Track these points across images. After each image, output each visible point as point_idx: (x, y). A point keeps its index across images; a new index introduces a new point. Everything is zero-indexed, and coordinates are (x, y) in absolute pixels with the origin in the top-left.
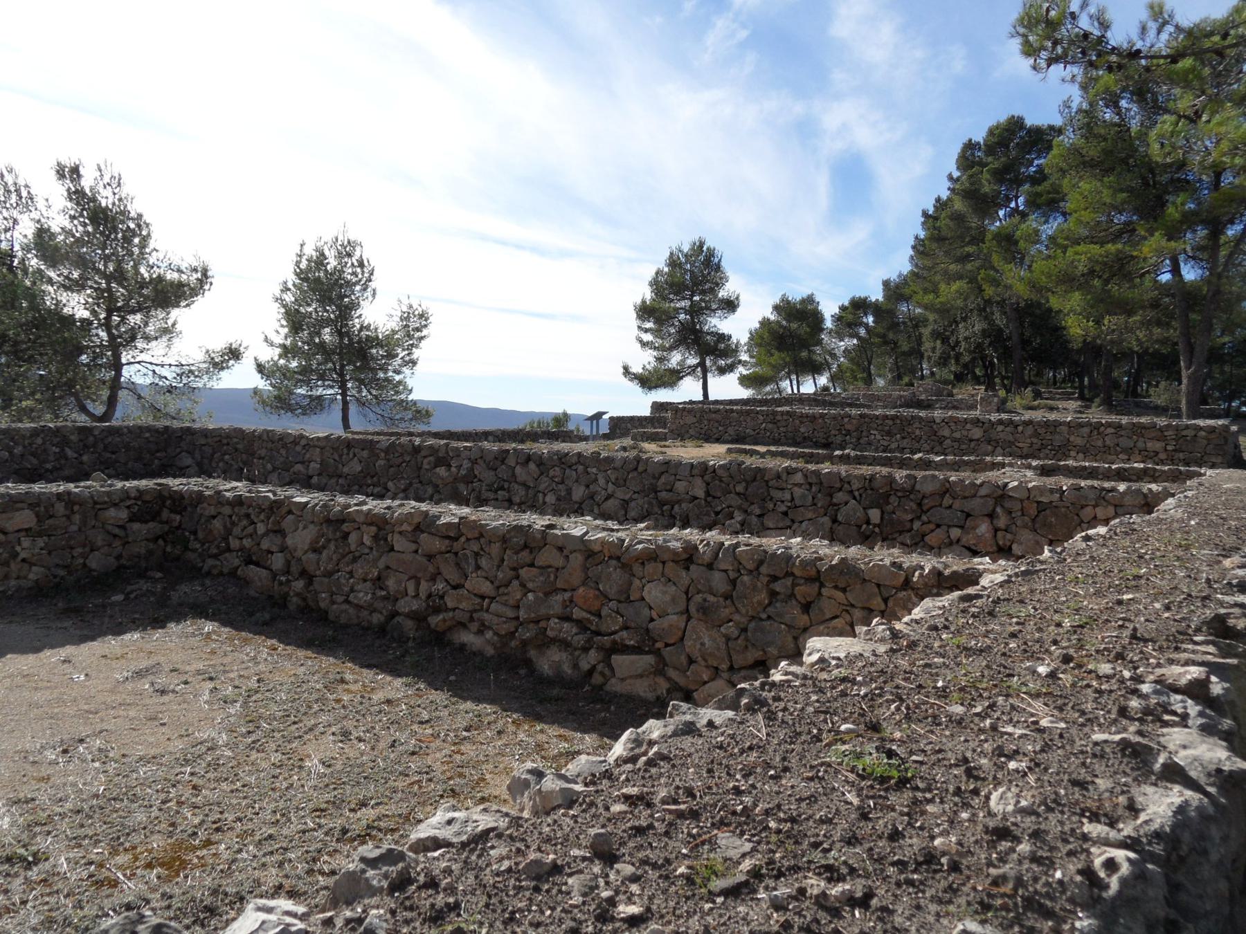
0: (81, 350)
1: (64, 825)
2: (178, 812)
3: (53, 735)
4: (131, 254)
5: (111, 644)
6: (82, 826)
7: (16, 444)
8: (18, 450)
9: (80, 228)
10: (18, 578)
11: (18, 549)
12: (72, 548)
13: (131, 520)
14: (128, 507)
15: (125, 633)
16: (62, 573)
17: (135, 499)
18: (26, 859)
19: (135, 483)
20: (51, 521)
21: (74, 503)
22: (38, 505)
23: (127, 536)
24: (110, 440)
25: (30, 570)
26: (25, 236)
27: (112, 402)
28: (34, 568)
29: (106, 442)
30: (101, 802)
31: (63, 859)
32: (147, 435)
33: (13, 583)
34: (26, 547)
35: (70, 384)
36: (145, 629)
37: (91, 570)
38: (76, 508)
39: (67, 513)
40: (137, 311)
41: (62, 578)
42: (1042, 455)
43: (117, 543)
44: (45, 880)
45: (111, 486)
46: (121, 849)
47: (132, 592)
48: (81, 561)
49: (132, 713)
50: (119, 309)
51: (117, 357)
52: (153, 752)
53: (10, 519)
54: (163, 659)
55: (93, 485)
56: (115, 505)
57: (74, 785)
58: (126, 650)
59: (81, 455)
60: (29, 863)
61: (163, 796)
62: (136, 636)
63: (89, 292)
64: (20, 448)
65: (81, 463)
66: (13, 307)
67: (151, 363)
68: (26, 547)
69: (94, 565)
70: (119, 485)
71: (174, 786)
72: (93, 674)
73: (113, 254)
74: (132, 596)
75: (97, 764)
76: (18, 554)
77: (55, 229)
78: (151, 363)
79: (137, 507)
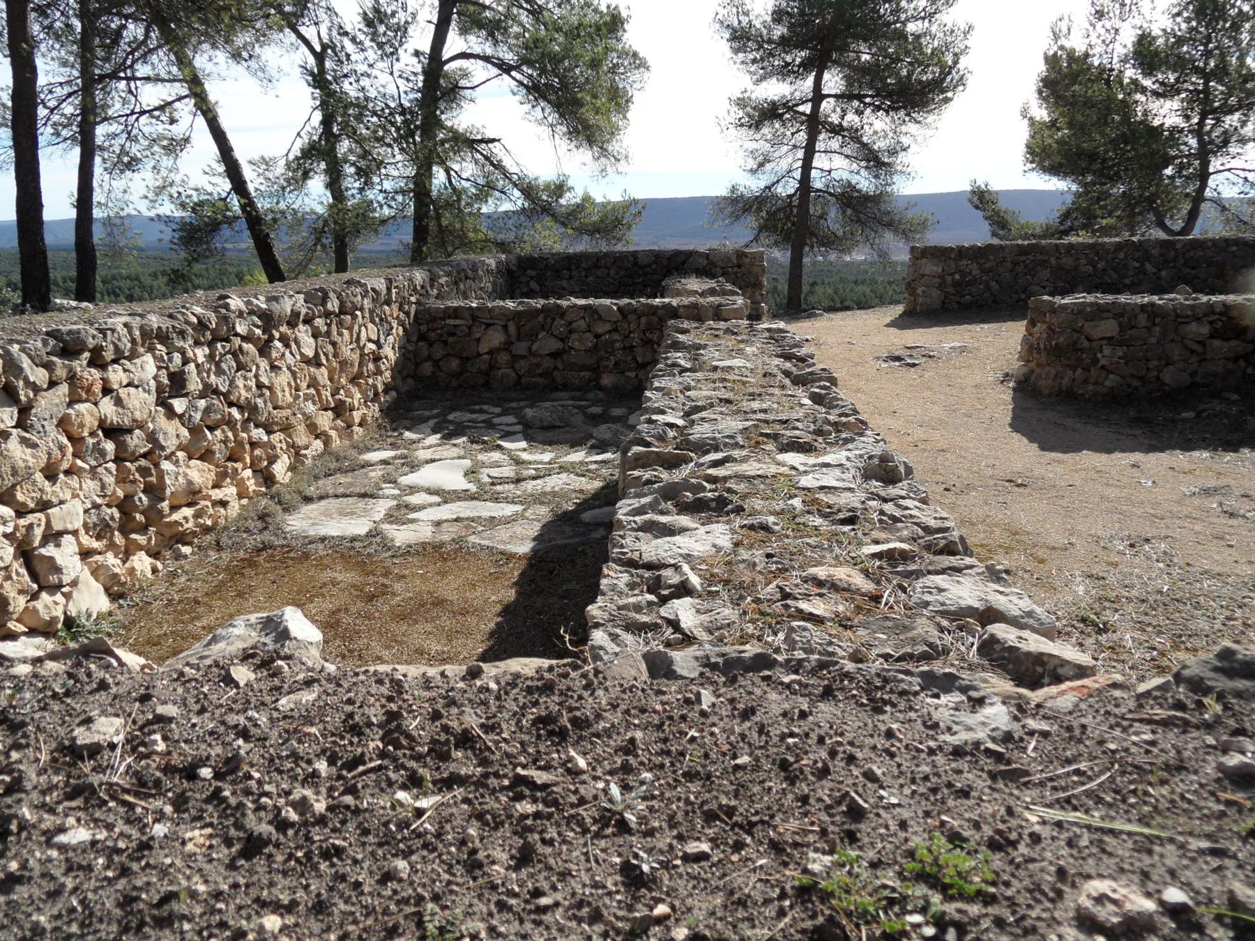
0: (1167, 161)
1: (1130, 608)
2: (1243, 633)
3: (1121, 529)
4: (1238, 43)
5: (1178, 458)
6: (1146, 614)
7: (1100, 258)
8: (1101, 265)
9: (1184, 26)
10: (1096, 383)
11: (1099, 355)
12: (1148, 360)
13: (1212, 336)
14: (1211, 323)
15: (1194, 449)
16: (1136, 383)
17: (1220, 314)
18: (1097, 625)
19: (1222, 297)
20: (1133, 332)
21: (1156, 316)
22: (1122, 315)
23: (1205, 353)
24: (1192, 254)
25: (1107, 378)
26: (1125, 46)
27: (1193, 215)
28: (1111, 376)
29: (1187, 256)
30: (1167, 600)
31: (1128, 636)
32: (1234, 248)
33: (1091, 387)
34: (1107, 355)
35: (1151, 200)
36: (1215, 450)
37: (1164, 384)
38: (1158, 320)
39: (1149, 324)
40: (1237, 110)
41: (1136, 388)
42: (1154, 823)
43: (1194, 359)
44: (1113, 648)
45: (1195, 299)
46: (1183, 647)
47: (1202, 411)
48: (1156, 373)
49: (1197, 528)
50: (1214, 111)
51: (1205, 164)
52: (1218, 569)
53: (1096, 327)
54: (1232, 483)
55: (1178, 298)
56: (1198, 319)
57: (1140, 577)
58: (1194, 466)
59: (1160, 270)
60: (1100, 629)
61: (1228, 613)
62: (1206, 454)
63: (1183, 95)
64: (1103, 263)
65: (1159, 278)
66: (1106, 124)
67: (1244, 170)
68: (1107, 355)
69: (1167, 379)
70: (1204, 299)
71: (1240, 607)
72: (1160, 483)
73: (1216, 48)
74: (1204, 415)
75: (1161, 565)
76: (1098, 361)
77: (1156, 32)
78: (1244, 170)
79: (1220, 324)
